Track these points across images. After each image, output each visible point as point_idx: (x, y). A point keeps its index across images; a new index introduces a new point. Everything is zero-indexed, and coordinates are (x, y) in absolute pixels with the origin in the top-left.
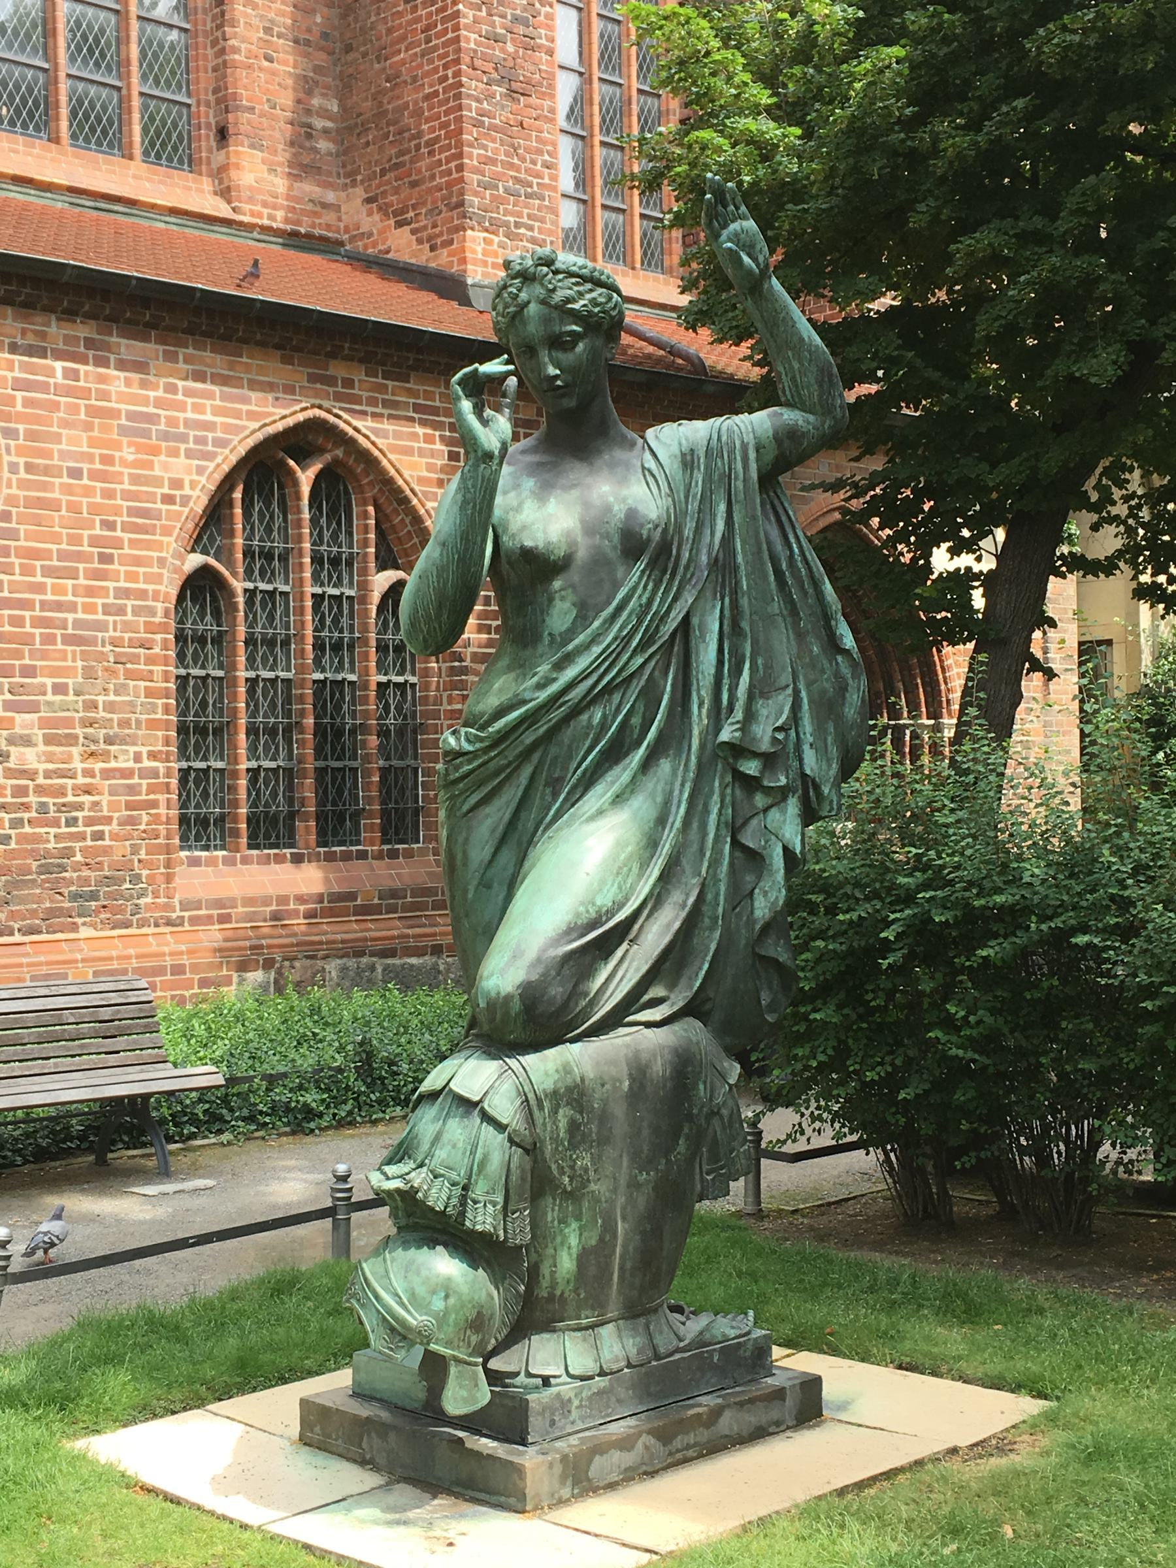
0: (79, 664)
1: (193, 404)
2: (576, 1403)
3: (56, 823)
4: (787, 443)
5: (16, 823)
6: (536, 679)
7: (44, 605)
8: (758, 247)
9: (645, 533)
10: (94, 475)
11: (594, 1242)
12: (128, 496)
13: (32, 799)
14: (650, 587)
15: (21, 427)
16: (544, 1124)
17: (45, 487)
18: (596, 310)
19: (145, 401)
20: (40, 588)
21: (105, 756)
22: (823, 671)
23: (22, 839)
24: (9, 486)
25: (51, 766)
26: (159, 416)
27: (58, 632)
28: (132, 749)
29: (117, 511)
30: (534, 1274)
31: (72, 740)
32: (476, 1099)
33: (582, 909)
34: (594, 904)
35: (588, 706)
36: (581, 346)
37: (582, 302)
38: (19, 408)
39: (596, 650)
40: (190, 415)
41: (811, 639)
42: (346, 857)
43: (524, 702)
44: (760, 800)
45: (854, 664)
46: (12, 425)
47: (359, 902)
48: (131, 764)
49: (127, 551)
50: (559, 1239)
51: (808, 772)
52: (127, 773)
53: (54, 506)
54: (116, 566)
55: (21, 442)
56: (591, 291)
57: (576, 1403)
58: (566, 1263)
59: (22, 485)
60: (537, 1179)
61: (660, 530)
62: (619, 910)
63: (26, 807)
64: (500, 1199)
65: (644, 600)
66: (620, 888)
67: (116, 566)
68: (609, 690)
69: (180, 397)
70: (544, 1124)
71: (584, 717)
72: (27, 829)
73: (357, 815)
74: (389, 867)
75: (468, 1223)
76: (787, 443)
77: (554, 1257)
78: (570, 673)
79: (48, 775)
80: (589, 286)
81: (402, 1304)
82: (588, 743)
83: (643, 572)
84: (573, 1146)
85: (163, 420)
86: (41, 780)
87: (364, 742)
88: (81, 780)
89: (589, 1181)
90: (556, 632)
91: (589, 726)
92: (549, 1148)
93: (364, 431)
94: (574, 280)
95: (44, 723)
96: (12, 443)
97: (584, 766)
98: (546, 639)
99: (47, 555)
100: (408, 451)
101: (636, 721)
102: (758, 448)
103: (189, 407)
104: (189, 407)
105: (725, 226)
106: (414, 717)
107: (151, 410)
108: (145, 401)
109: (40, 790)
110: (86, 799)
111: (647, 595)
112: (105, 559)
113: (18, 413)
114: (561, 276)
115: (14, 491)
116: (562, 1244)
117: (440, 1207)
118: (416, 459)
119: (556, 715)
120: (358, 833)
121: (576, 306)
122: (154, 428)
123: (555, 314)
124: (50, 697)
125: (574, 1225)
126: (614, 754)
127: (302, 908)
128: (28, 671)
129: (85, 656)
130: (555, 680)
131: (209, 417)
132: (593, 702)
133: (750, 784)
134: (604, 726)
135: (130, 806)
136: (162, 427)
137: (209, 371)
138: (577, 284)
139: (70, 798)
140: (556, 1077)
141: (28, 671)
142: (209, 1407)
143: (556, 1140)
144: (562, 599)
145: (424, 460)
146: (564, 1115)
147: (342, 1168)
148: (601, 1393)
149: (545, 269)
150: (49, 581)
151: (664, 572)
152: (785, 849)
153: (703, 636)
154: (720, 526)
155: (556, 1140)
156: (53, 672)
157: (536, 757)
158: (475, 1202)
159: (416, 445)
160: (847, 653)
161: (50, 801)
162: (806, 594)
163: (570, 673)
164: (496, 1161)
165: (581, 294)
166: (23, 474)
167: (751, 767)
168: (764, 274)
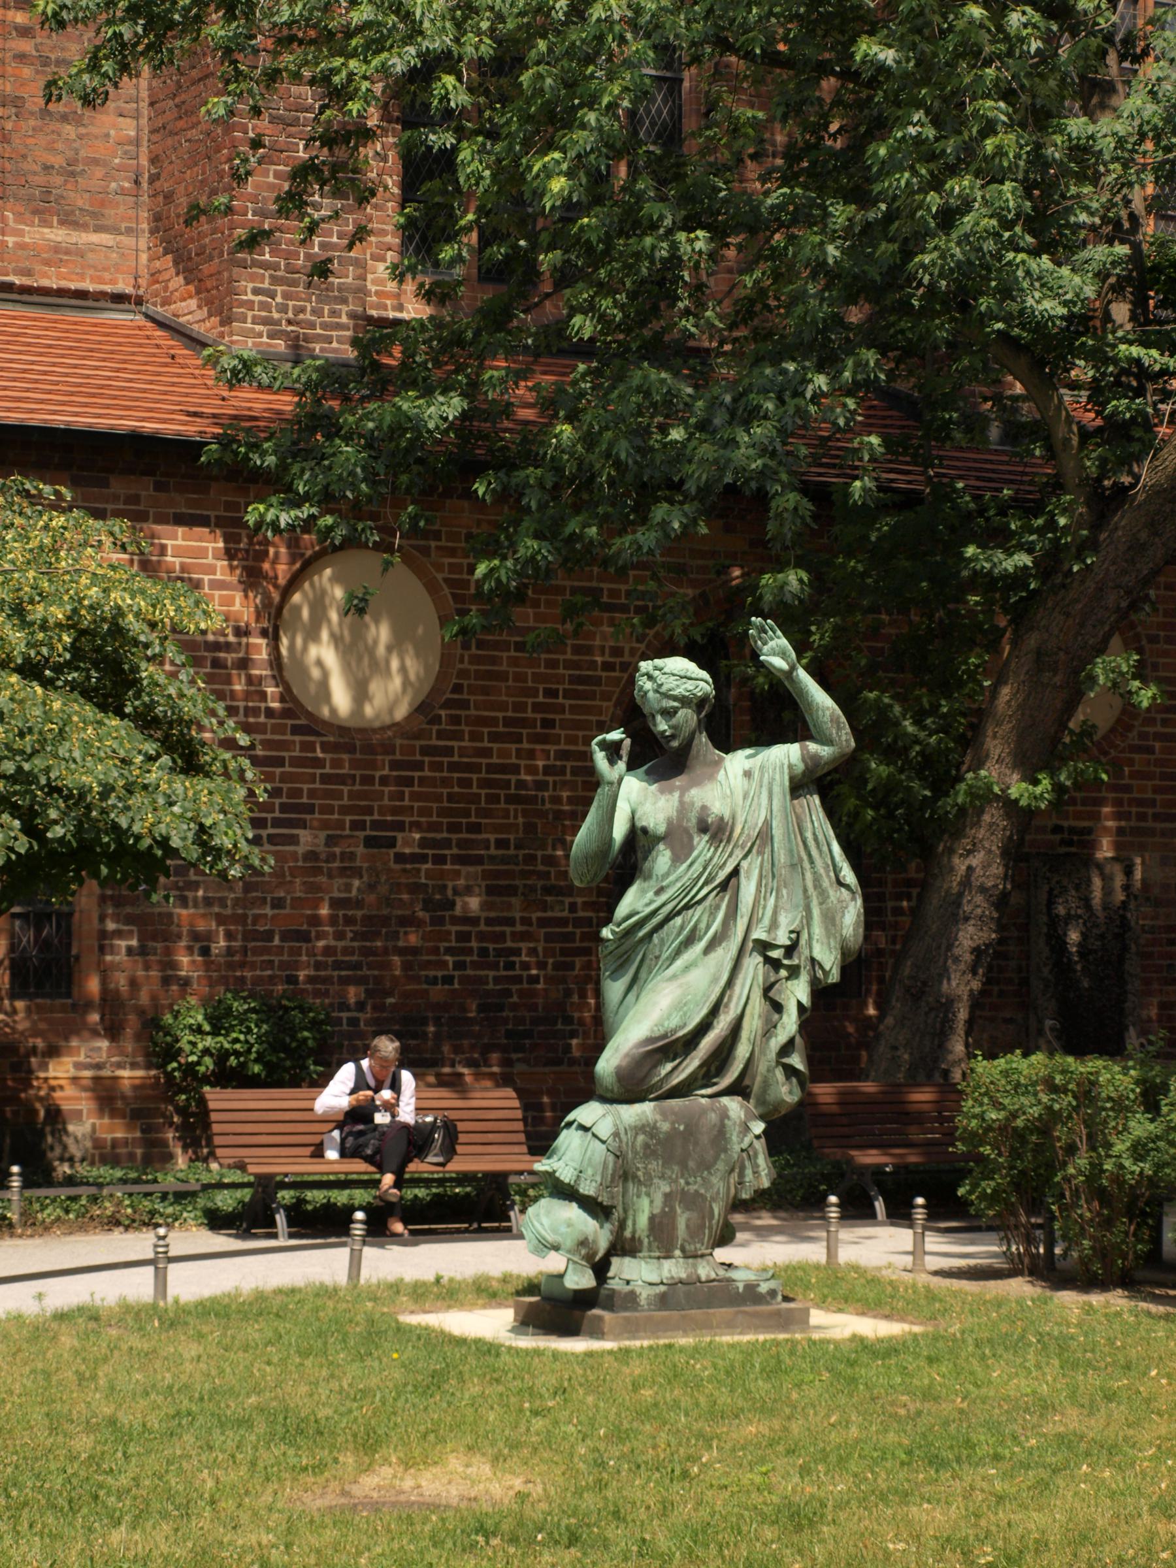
0: (521, 820)
3: (495, 966)
5: (459, 966)
7: (491, 768)
12: (569, 665)
13: (474, 944)
17: (494, 661)
20: (487, 753)
21: (545, 907)
23: (463, 980)
24: (462, 661)
25: (493, 914)
27: (502, 793)
28: (567, 900)
29: (559, 679)
30: (622, 1225)
31: (511, 891)
48: (566, 914)
49: (567, 716)
52: (563, 922)
53: (502, 676)
54: (557, 731)
58: (643, 1221)
59: (475, 660)
60: (623, 1172)
63: (469, 951)
67: (557, 731)
68: (687, 907)
72: (469, 972)
78: (664, 897)
79: (489, 922)
84: (646, 1156)
86: (483, 927)
88: (519, 928)
95: (486, 875)
99: (493, 722)
101: (703, 925)
109: (482, 937)
110: (524, 946)
112: (548, 724)
115: (466, 665)
124: (493, 851)
126: (690, 941)
128: (475, 828)
129: (525, 813)
132: (679, 913)
133: (775, 964)
134: (682, 928)
135: (564, 952)
139: (509, 944)
141: (475, 828)
143: (636, 1153)
150: (495, 746)
152: (799, 1004)
153: (748, 878)
155: (636, 1153)
156: (497, 829)
160: (847, 887)
161: (491, 946)
163: (664, 897)
166: (474, 650)
167: (775, 954)
168: (793, 668)
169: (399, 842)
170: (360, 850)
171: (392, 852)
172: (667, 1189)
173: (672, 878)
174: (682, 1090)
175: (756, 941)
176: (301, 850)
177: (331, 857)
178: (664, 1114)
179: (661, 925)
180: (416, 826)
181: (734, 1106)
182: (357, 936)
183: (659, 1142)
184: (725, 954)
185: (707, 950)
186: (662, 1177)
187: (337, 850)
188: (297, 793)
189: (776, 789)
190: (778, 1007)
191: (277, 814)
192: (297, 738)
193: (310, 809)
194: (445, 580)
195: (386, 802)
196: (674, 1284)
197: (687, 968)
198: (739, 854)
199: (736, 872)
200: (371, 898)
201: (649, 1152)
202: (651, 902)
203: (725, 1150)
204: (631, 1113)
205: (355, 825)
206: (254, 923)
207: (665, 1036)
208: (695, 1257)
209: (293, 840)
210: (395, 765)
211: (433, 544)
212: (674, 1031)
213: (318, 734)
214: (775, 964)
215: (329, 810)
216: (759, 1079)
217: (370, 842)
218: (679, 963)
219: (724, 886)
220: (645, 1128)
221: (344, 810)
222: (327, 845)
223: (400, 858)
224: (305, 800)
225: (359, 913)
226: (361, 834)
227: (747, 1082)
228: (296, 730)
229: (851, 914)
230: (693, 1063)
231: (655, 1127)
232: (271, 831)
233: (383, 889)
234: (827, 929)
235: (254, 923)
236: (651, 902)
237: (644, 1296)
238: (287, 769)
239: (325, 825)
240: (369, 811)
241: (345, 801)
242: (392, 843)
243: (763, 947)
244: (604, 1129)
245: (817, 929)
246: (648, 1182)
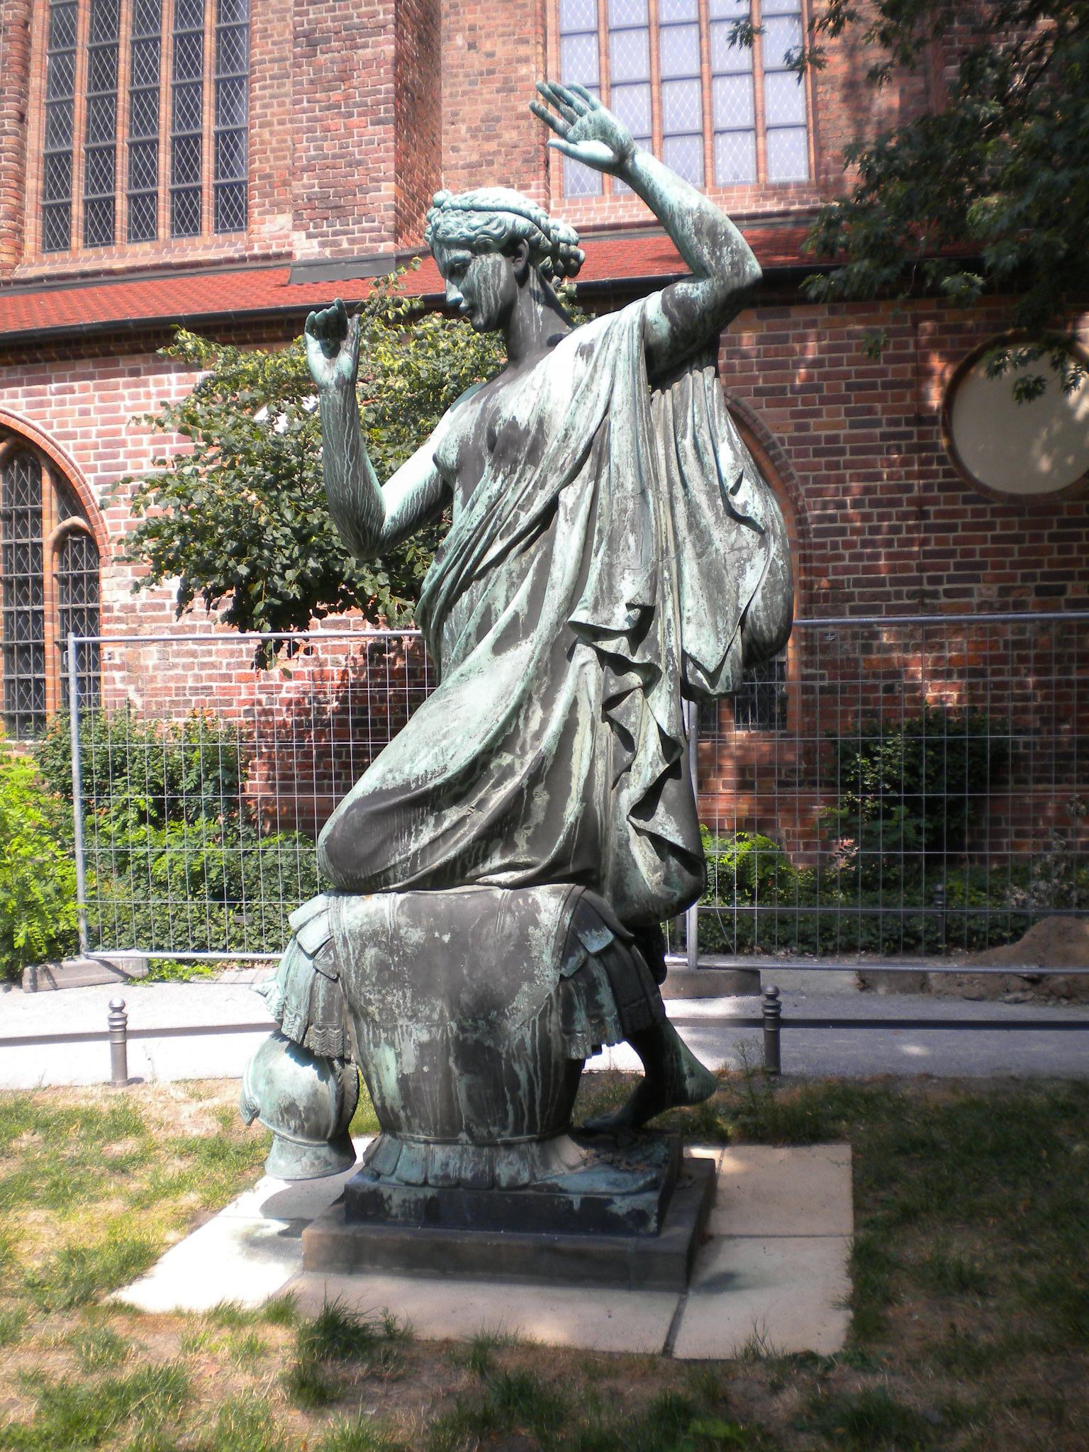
33: (389, 776)
34: (401, 771)
132: (465, 586)
133: (616, 664)
134: (471, 610)
143: (364, 977)
147: (117, 1004)
155: (364, 977)
169: (1069, 590)
171: (1062, 599)
172: (425, 1037)
174: (451, 874)
176: (975, 600)
178: (415, 916)
183: (405, 959)
184: (525, 653)
185: (499, 647)
186: (414, 1017)
187: (1010, 599)
188: (970, 553)
189: (622, 366)
190: (627, 740)
192: (969, 507)
193: (981, 566)
195: (1055, 556)
196: (451, 1186)
198: (554, 481)
199: (552, 507)
200: (1043, 639)
201: (386, 976)
203: (531, 978)
205: (1025, 578)
207: (405, 787)
208: (493, 1145)
209: (967, 593)
210: (1062, 524)
212: (424, 778)
213: (987, 502)
214: (616, 664)
216: (612, 858)
217: (1040, 591)
221: (1015, 565)
222: (1000, 595)
225: (1032, 653)
226: (1032, 585)
229: (755, 578)
231: (395, 935)
232: (947, 586)
234: (711, 600)
237: (397, 1199)
239: (997, 579)
240: (1038, 564)
241: (1016, 558)
243: (593, 634)
245: (693, 601)
246: (388, 1023)
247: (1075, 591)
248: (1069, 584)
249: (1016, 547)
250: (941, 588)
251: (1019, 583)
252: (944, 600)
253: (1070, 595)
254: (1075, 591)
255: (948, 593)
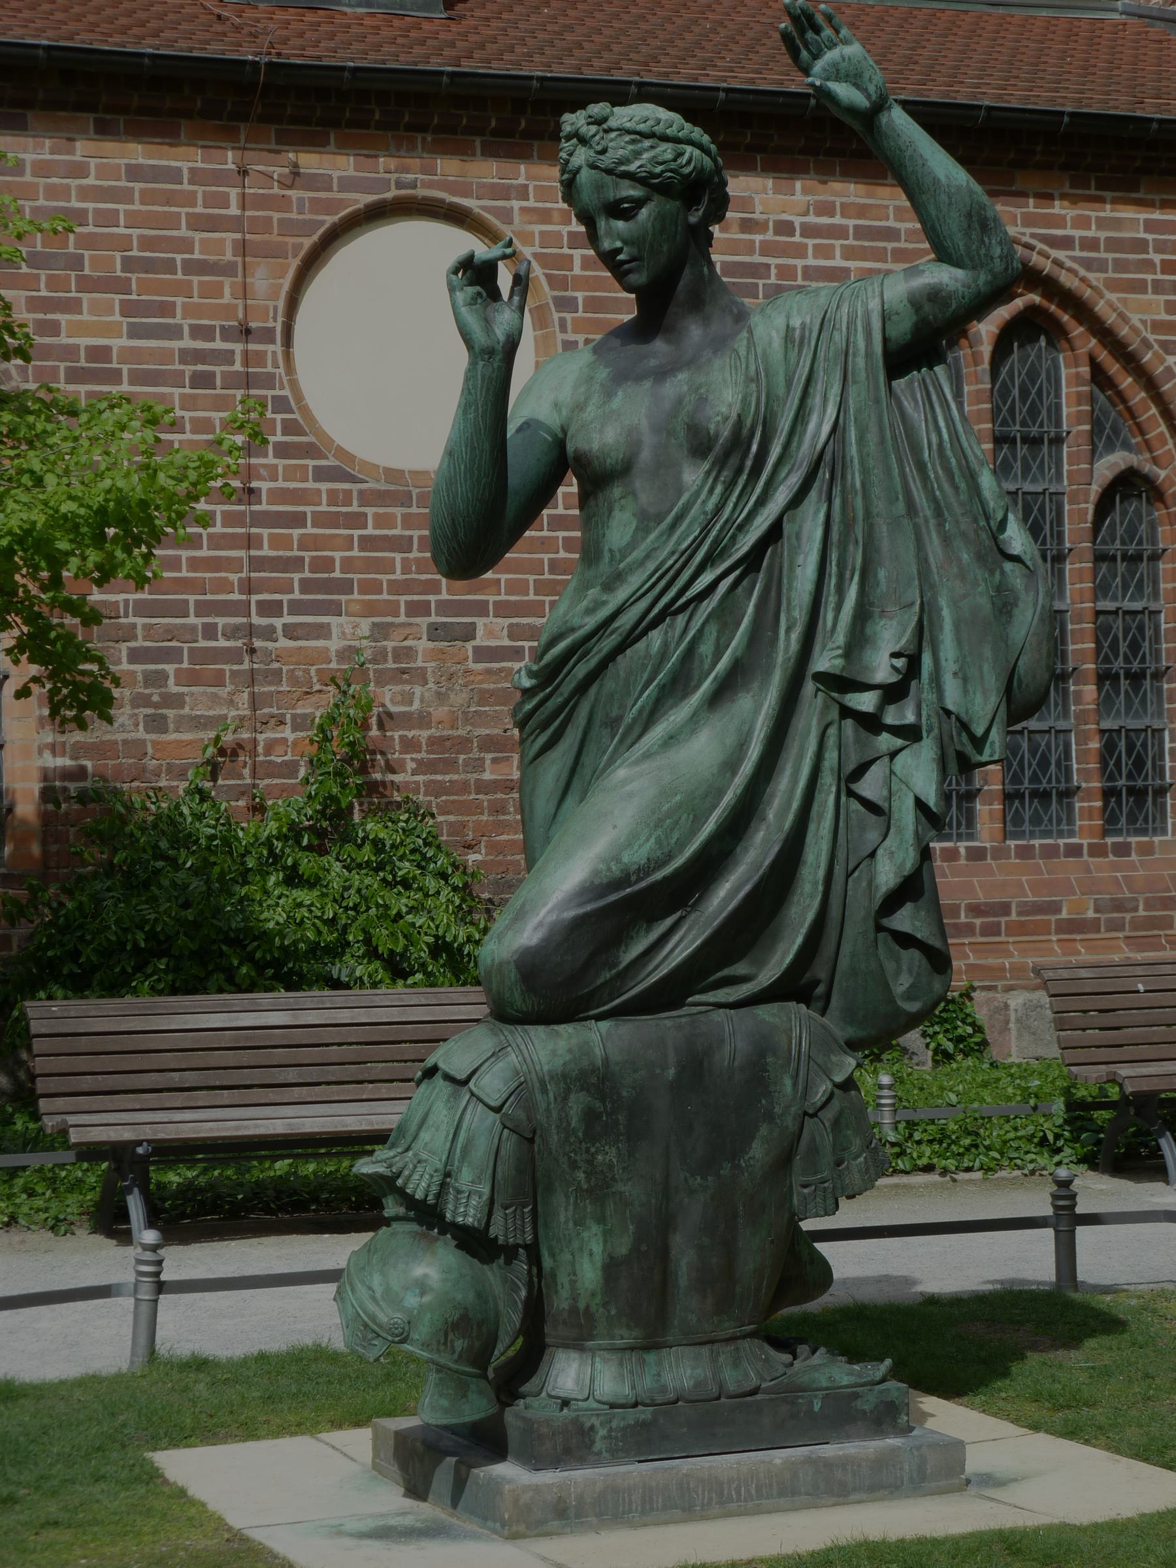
1: (815, 246)
2: (602, 1432)
4: (927, 308)
6: (585, 603)
8: (866, 75)
9: (712, 427)
10: (231, 381)
11: (624, 1250)
14: (719, 489)
15: (580, 295)
16: (548, 1110)
18: (659, 169)
19: (750, 248)
22: (976, 584)
26: (768, 266)
32: (462, 1076)
35: (645, 633)
36: (644, 212)
37: (637, 163)
38: (577, 270)
39: (651, 566)
40: (811, 261)
41: (958, 543)
42: (1050, 852)
43: (573, 630)
44: (886, 741)
45: (1031, 573)
46: (569, 294)
47: (1064, 915)
50: (576, 1244)
51: (950, 707)
55: (580, 314)
56: (652, 147)
57: (602, 1432)
58: (589, 1274)
60: (529, 1168)
61: (731, 422)
62: (655, 870)
64: (486, 1191)
65: (710, 506)
66: (659, 842)
69: (797, 238)
70: (548, 1110)
71: (641, 645)
73: (1068, 794)
74: (1115, 867)
75: (448, 1215)
76: (927, 308)
77: (573, 1264)
80: (647, 143)
81: (374, 1299)
82: (645, 676)
83: (708, 473)
85: (773, 271)
87: (1078, 695)
89: (614, 1179)
90: (615, 547)
91: (647, 655)
92: (554, 1139)
93: (1069, 263)
94: (627, 138)
96: (568, 316)
97: (639, 703)
98: (607, 556)
100: (1139, 287)
102: (885, 318)
103: (810, 251)
104: (810, 251)
105: (816, 57)
106: (1158, 658)
107: (757, 259)
108: (750, 248)
111: (714, 499)
113: (575, 277)
114: (613, 135)
116: (581, 1249)
117: (419, 1195)
118: (1150, 296)
119: (608, 643)
120: (1071, 821)
121: (632, 167)
122: (761, 282)
123: (608, 179)
125: (595, 1228)
126: (678, 684)
127: (978, 922)
130: (604, 603)
131: (838, 262)
132: (654, 624)
136: (773, 280)
137: (838, 201)
138: (633, 142)
140: (568, 1057)
142: (324, 1436)
144: (622, 509)
145: (1163, 298)
146: (577, 1103)
148: (644, 1425)
149: (594, 128)
151: (739, 471)
152: (920, 804)
154: (831, 412)
157: (593, 691)
158: (459, 1192)
159: (1149, 277)
162: (956, 488)
163: (621, 594)
164: (482, 1149)
165: (637, 154)
167: (866, 702)
169: (480, 632)
170: (423, 644)
171: (469, 646)
173: (637, 554)
175: (820, 677)
176: (334, 644)
177: (380, 656)
179: (620, 648)
180: (503, 610)
181: (791, 1021)
182: (423, 767)
184: (757, 707)
185: (717, 699)
187: (389, 645)
191: (297, 595)
192: (324, 486)
193: (345, 587)
194: (535, 255)
197: (670, 740)
202: (598, 605)
204: (549, 1048)
206: (268, 752)
209: (322, 631)
211: (516, 204)
212: (645, 870)
213: (353, 479)
215: (376, 587)
217: (435, 632)
218: (658, 731)
219: (752, 561)
220: (594, 1080)
221: (397, 588)
222: (372, 638)
223: (482, 654)
224: (337, 574)
226: (423, 621)
227: (820, 970)
228: (321, 474)
230: (685, 942)
233: (459, 698)
235: (268, 752)
236: (598, 605)
238: (310, 530)
239: (370, 610)
242: (468, 633)
244: (493, 1084)
247: (490, 634)
248: (480, 622)
249: (398, 557)
250: (278, 623)
251: (402, 618)
252: (284, 643)
253: (481, 640)
254: (490, 634)
255: (291, 632)
